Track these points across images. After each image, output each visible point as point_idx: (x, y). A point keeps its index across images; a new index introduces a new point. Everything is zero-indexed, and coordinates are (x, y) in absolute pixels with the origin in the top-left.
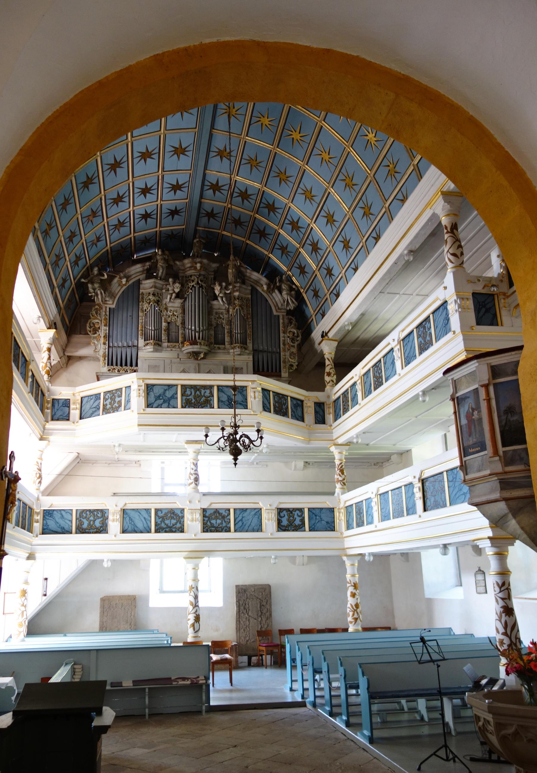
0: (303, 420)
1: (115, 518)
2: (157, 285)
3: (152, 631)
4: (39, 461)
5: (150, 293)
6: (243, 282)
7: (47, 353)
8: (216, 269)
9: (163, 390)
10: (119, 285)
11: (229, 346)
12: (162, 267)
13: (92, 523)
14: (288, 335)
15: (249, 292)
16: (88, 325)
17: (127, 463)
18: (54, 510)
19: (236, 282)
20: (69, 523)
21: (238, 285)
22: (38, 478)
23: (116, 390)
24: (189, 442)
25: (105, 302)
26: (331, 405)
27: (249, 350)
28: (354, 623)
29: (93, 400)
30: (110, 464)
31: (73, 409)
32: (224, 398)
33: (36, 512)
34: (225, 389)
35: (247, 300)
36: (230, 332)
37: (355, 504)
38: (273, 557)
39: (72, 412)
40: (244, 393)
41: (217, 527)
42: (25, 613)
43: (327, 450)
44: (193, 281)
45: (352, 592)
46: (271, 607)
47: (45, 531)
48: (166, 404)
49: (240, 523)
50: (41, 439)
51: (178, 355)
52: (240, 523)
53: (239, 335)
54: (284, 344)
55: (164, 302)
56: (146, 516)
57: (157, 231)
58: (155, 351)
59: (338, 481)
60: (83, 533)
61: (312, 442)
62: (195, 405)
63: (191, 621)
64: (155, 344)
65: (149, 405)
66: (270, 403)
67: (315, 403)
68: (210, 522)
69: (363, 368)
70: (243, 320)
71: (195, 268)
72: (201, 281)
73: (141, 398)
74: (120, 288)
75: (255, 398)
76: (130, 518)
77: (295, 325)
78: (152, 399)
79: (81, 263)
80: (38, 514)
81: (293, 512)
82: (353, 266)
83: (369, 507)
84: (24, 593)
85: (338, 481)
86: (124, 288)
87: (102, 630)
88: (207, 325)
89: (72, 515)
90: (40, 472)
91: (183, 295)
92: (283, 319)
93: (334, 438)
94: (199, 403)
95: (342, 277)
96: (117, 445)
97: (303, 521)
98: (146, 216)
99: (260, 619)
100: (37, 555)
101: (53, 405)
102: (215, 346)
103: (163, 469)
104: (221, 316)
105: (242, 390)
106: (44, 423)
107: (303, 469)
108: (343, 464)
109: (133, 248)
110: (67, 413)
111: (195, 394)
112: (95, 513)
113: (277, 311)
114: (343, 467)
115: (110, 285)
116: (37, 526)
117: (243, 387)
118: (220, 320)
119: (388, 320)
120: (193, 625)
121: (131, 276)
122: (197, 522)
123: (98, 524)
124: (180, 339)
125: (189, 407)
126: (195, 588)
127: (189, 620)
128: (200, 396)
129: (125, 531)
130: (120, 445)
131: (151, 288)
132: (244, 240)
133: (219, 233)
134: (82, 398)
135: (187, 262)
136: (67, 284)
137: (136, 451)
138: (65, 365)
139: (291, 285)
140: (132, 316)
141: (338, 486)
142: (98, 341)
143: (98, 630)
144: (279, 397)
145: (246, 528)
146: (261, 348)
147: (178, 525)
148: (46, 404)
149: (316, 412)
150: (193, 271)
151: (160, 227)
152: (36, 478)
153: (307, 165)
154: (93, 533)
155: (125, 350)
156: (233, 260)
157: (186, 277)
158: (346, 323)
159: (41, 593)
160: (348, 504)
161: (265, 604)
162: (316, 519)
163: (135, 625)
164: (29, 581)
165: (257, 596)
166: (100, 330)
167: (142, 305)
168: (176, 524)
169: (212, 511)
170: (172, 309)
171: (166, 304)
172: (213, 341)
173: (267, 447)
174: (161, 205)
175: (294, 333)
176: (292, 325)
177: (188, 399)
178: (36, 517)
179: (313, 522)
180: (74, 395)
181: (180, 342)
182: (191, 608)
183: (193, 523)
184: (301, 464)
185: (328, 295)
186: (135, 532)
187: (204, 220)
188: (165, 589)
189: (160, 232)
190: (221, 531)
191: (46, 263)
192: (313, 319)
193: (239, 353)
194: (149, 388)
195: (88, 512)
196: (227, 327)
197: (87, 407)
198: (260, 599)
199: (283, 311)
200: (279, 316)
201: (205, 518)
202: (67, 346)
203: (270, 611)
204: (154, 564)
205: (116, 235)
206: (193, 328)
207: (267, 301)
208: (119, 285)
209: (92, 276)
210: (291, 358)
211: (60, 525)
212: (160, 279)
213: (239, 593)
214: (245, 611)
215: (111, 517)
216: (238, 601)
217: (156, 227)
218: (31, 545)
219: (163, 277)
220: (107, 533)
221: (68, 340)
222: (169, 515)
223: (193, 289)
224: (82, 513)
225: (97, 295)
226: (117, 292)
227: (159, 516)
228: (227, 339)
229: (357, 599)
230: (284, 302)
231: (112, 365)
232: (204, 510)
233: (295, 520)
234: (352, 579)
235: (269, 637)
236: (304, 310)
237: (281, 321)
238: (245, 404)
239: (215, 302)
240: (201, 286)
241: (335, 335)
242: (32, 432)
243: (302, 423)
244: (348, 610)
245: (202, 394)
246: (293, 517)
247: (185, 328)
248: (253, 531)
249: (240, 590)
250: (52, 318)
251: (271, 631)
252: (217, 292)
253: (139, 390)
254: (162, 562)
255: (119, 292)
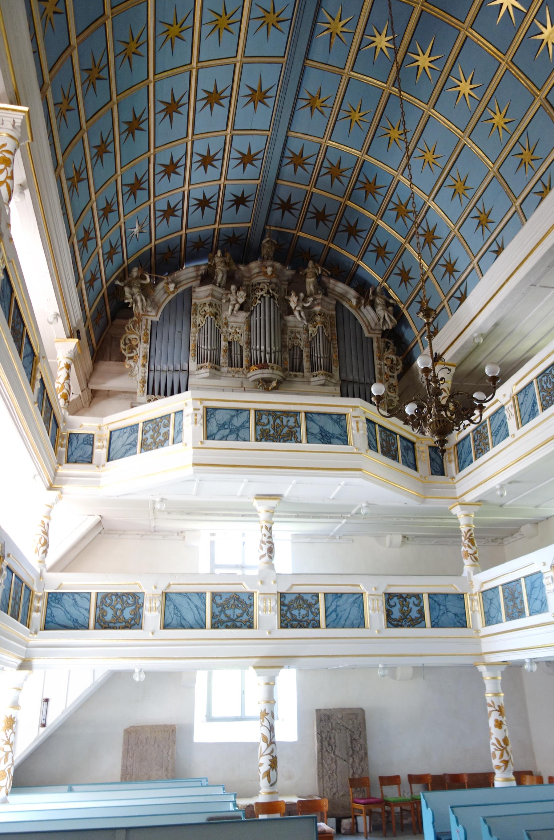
0: (415, 468)
1: (154, 605)
2: (215, 293)
3: (201, 782)
4: (46, 521)
5: (205, 304)
6: (326, 294)
7: (65, 370)
8: (291, 277)
9: (229, 417)
10: (165, 291)
11: (309, 374)
12: (222, 271)
13: (119, 613)
14: (385, 362)
15: (333, 307)
16: (122, 341)
17: (166, 534)
18: (63, 593)
19: (317, 293)
20: (85, 613)
21: (320, 297)
22: (43, 545)
23: (161, 418)
24: (259, 497)
25: (146, 313)
26: (452, 450)
27: (336, 380)
28: (503, 768)
29: (127, 435)
30: (142, 535)
31: (99, 447)
32: (315, 429)
33: (37, 596)
34: (316, 417)
35: (330, 318)
36: (311, 357)
37: (502, 585)
38: (380, 666)
39: (96, 451)
40: (343, 423)
41: (301, 621)
42: (10, 755)
43: (447, 513)
44: (262, 290)
45: (496, 720)
46: (366, 742)
47: (50, 624)
48: (234, 436)
49: (334, 615)
50: (51, 488)
51: (242, 383)
52: (334, 615)
53: (322, 360)
54: (380, 374)
55: (224, 316)
56: (199, 604)
57: (214, 229)
58: (212, 376)
59: (467, 555)
60: (105, 628)
61: (428, 500)
62: (274, 437)
63: (265, 768)
64: (211, 367)
65: (209, 436)
66: (376, 440)
67: (430, 447)
68: (291, 613)
69: (517, 384)
70: (328, 341)
71: (265, 274)
72: (273, 290)
73: (198, 425)
74: (166, 296)
75: (358, 429)
76: (175, 606)
77: (394, 350)
78: (213, 427)
79: (117, 258)
80: (39, 598)
81: (407, 599)
82: (494, 247)
83: (533, 588)
84: (11, 723)
85: (467, 555)
86: (172, 296)
87: (125, 779)
88: (280, 346)
89: (90, 601)
90: (45, 536)
91: (249, 308)
92: (378, 342)
93: (458, 495)
94: (280, 435)
95: (473, 268)
96: (158, 500)
97: (421, 612)
98: (204, 203)
99: (351, 760)
100: (35, 662)
101: (70, 442)
102: (291, 373)
103: (212, 543)
104: (298, 336)
105: (339, 419)
106: (56, 466)
107: (400, 547)
108: (472, 531)
109: (183, 253)
110: (90, 452)
111: (274, 422)
112: (125, 598)
113: (369, 333)
114: (473, 535)
115: (154, 291)
116: (37, 618)
117: (341, 415)
118: (297, 341)
119: (526, 336)
120: (268, 774)
121: (180, 282)
122: (273, 613)
123: (127, 614)
124: (245, 363)
125: (266, 441)
126: (270, 714)
127: (261, 765)
128: (282, 426)
129: (168, 625)
130: (162, 500)
131: (207, 297)
132: (326, 243)
133: (294, 234)
134: (111, 432)
135: (254, 266)
136: (97, 284)
137: (182, 512)
138: (88, 403)
139: (388, 299)
140: (181, 332)
141: (467, 562)
142: (136, 362)
143: (118, 779)
144: (387, 434)
145: (342, 622)
146: (350, 378)
147: (245, 617)
148: (60, 440)
149: (432, 459)
150: (263, 278)
151: (220, 223)
152: (40, 545)
153: (433, 108)
154: (119, 628)
155: (171, 375)
156: (312, 268)
157: (252, 286)
158: (475, 335)
159: (37, 722)
160: (486, 587)
161: (357, 737)
162: (440, 609)
163: (173, 771)
164: (20, 703)
165: (346, 725)
166: (138, 349)
167: (195, 318)
168: (242, 615)
169: (293, 597)
170: (235, 325)
171: (226, 318)
172: (288, 366)
173: (367, 506)
174: (225, 186)
175: (392, 360)
176: (390, 350)
177: (265, 430)
178: (36, 604)
179: (435, 614)
180: (100, 428)
181: (244, 367)
182: (264, 745)
183: (266, 613)
184: (398, 539)
185: (445, 302)
186: (183, 627)
187: (277, 214)
188: (214, 714)
189: (219, 230)
190: (307, 627)
191: (71, 234)
192: (417, 342)
193: (323, 382)
194: (210, 413)
195: (114, 597)
196: (305, 352)
197: (117, 444)
198: (350, 731)
199: (377, 332)
200: (372, 339)
201: (283, 608)
202: (91, 375)
203: (364, 748)
204: (201, 676)
205: (163, 228)
206: (263, 347)
207: (356, 319)
208: (165, 292)
209: (130, 279)
210: (390, 392)
211: (71, 616)
212: (219, 286)
213: (321, 720)
214: (329, 749)
215: (147, 604)
216: (320, 733)
217: (215, 224)
218: (27, 647)
219: (222, 284)
220: (141, 628)
221: (93, 367)
222: (232, 602)
223: (262, 299)
224: (105, 599)
225: (136, 302)
226: (162, 301)
227: (216, 604)
228: (306, 365)
229: (505, 731)
230: (379, 320)
231: (153, 393)
232: (282, 595)
233: (411, 611)
234: (494, 699)
235: (365, 788)
236: (403, 335)
237: (375, 345)
238: (345, 438)
239: (290, 318)
240: (273, 297)
241: (454, 356)
242: (37, 473)
243: (415, 472)
244: (492, 748)
245: (285, 423)
246: (408, 607)
247: (251, 349)
248: (353, 626)
249: (323, 717)
250: (75, 325)
251: (368, 778)
252: (293, 305)
253: (196, 415)
254: (210, 675)
255: (164, 301)
